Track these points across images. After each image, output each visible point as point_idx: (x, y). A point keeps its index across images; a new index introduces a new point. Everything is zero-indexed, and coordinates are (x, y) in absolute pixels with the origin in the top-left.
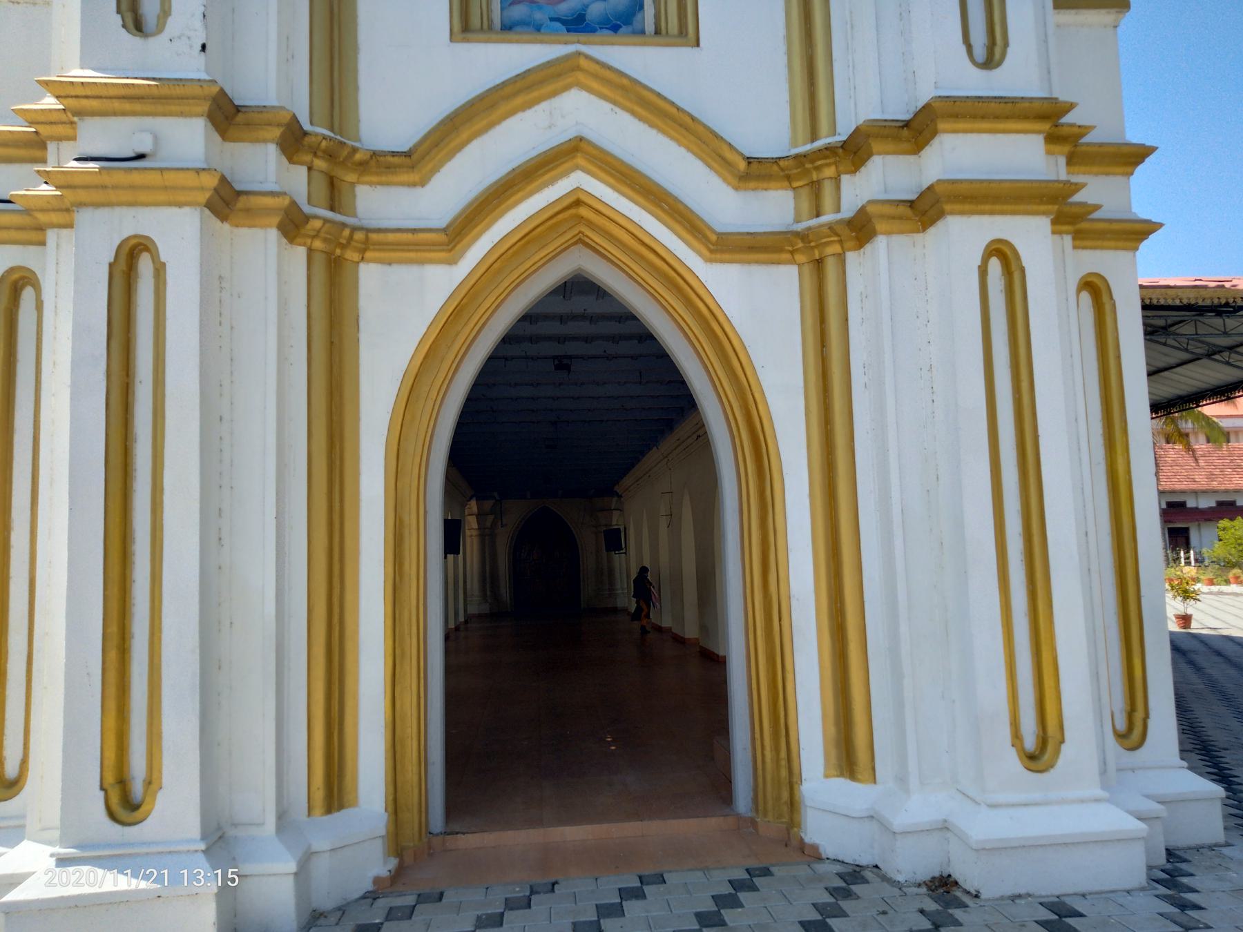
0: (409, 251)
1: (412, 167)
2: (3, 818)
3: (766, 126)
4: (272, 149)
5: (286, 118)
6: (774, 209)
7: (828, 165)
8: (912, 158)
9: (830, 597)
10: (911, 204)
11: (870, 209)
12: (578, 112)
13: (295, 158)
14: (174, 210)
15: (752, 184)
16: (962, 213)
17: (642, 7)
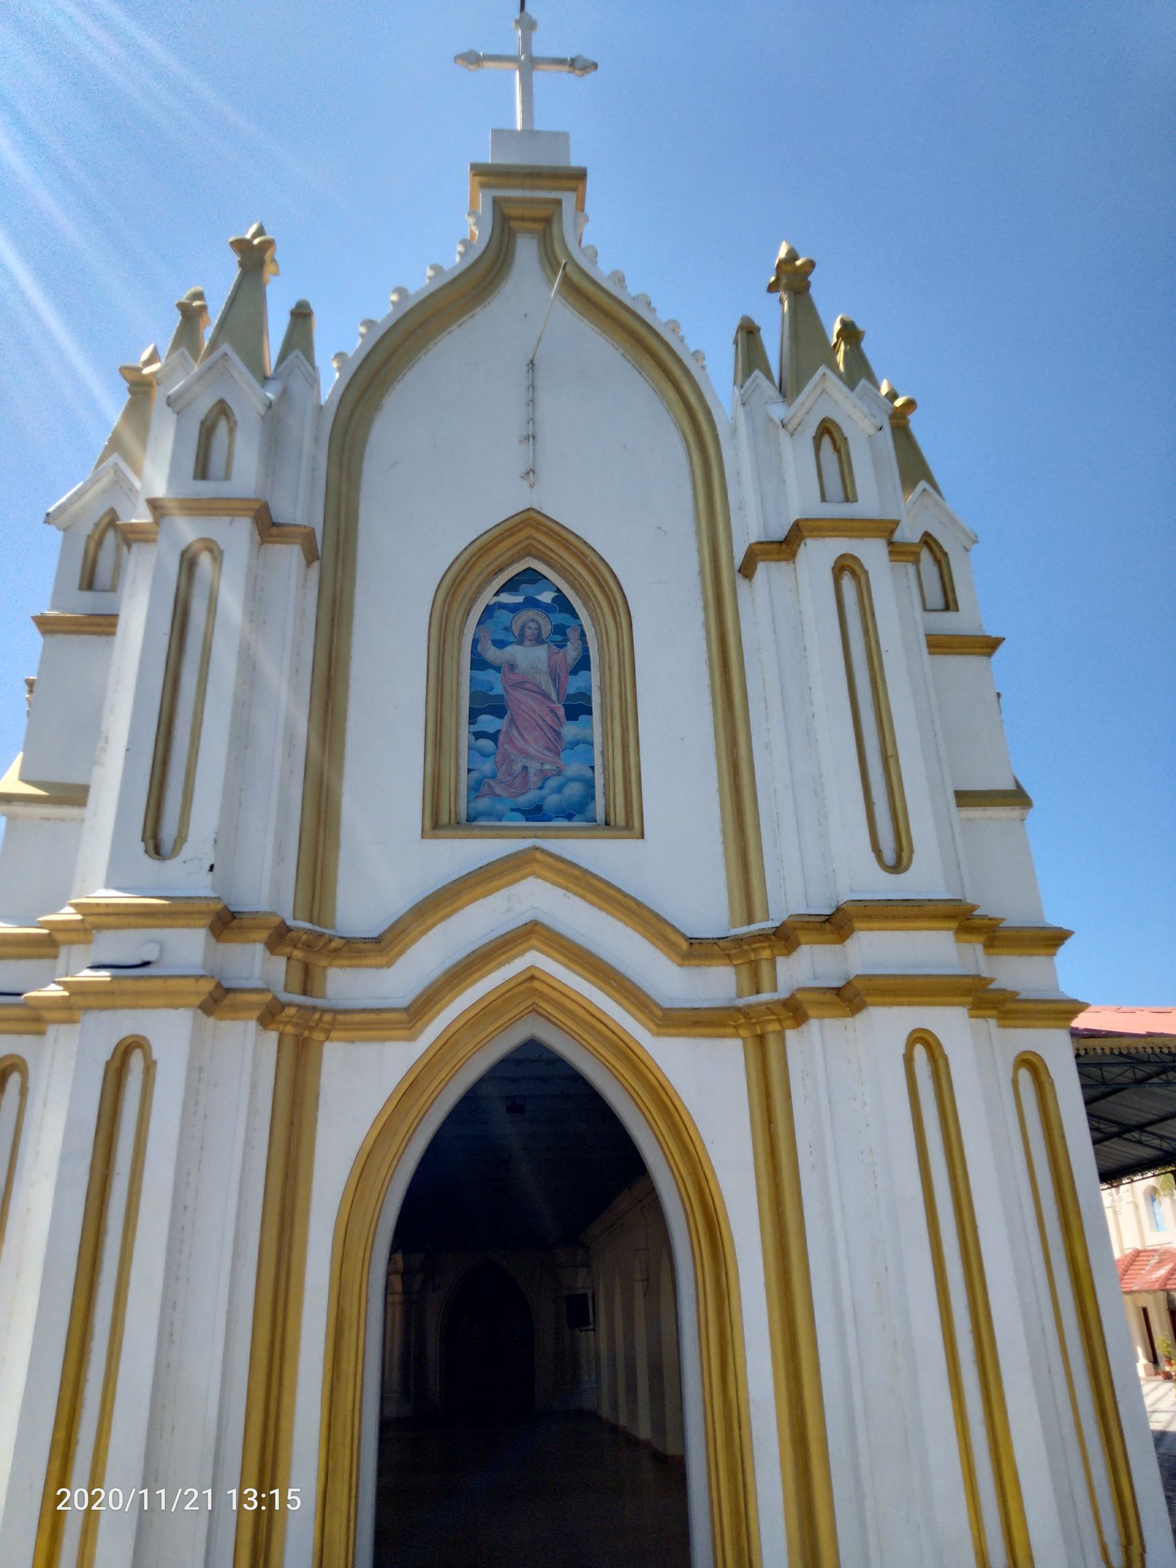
0: (372, 1029)
1: (381, 952)
2: (261, 1535)
3: (705, 908)
4: (260, 948)
5: (275, 921)
6: (716, 984)
7: (764, 948)
8: (837, 947)
9: (790, 1402)
10: (838, 991)
11: (799, 996)
12: (536, 898)
13: (277, 951)
14: (171, 1012)
15: (695, 962)
16: (883, 1004)
17: (593, 798)
